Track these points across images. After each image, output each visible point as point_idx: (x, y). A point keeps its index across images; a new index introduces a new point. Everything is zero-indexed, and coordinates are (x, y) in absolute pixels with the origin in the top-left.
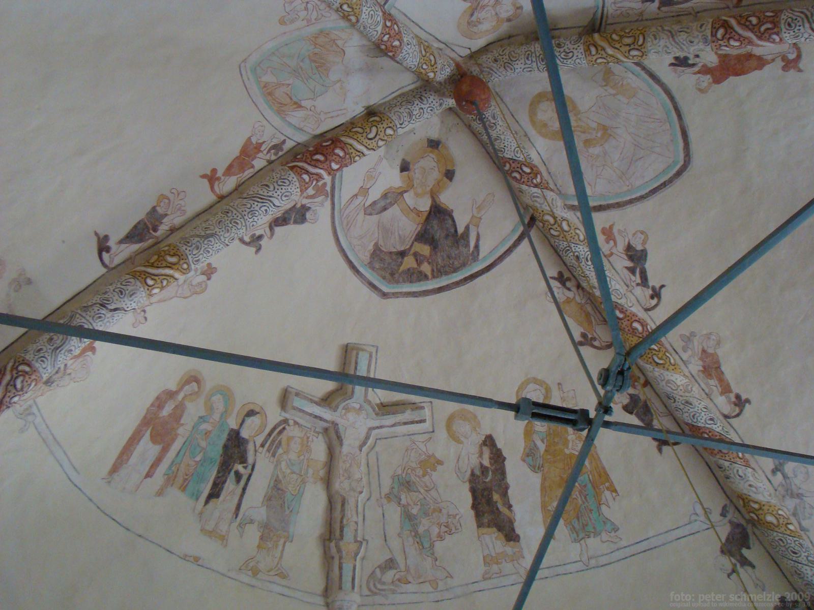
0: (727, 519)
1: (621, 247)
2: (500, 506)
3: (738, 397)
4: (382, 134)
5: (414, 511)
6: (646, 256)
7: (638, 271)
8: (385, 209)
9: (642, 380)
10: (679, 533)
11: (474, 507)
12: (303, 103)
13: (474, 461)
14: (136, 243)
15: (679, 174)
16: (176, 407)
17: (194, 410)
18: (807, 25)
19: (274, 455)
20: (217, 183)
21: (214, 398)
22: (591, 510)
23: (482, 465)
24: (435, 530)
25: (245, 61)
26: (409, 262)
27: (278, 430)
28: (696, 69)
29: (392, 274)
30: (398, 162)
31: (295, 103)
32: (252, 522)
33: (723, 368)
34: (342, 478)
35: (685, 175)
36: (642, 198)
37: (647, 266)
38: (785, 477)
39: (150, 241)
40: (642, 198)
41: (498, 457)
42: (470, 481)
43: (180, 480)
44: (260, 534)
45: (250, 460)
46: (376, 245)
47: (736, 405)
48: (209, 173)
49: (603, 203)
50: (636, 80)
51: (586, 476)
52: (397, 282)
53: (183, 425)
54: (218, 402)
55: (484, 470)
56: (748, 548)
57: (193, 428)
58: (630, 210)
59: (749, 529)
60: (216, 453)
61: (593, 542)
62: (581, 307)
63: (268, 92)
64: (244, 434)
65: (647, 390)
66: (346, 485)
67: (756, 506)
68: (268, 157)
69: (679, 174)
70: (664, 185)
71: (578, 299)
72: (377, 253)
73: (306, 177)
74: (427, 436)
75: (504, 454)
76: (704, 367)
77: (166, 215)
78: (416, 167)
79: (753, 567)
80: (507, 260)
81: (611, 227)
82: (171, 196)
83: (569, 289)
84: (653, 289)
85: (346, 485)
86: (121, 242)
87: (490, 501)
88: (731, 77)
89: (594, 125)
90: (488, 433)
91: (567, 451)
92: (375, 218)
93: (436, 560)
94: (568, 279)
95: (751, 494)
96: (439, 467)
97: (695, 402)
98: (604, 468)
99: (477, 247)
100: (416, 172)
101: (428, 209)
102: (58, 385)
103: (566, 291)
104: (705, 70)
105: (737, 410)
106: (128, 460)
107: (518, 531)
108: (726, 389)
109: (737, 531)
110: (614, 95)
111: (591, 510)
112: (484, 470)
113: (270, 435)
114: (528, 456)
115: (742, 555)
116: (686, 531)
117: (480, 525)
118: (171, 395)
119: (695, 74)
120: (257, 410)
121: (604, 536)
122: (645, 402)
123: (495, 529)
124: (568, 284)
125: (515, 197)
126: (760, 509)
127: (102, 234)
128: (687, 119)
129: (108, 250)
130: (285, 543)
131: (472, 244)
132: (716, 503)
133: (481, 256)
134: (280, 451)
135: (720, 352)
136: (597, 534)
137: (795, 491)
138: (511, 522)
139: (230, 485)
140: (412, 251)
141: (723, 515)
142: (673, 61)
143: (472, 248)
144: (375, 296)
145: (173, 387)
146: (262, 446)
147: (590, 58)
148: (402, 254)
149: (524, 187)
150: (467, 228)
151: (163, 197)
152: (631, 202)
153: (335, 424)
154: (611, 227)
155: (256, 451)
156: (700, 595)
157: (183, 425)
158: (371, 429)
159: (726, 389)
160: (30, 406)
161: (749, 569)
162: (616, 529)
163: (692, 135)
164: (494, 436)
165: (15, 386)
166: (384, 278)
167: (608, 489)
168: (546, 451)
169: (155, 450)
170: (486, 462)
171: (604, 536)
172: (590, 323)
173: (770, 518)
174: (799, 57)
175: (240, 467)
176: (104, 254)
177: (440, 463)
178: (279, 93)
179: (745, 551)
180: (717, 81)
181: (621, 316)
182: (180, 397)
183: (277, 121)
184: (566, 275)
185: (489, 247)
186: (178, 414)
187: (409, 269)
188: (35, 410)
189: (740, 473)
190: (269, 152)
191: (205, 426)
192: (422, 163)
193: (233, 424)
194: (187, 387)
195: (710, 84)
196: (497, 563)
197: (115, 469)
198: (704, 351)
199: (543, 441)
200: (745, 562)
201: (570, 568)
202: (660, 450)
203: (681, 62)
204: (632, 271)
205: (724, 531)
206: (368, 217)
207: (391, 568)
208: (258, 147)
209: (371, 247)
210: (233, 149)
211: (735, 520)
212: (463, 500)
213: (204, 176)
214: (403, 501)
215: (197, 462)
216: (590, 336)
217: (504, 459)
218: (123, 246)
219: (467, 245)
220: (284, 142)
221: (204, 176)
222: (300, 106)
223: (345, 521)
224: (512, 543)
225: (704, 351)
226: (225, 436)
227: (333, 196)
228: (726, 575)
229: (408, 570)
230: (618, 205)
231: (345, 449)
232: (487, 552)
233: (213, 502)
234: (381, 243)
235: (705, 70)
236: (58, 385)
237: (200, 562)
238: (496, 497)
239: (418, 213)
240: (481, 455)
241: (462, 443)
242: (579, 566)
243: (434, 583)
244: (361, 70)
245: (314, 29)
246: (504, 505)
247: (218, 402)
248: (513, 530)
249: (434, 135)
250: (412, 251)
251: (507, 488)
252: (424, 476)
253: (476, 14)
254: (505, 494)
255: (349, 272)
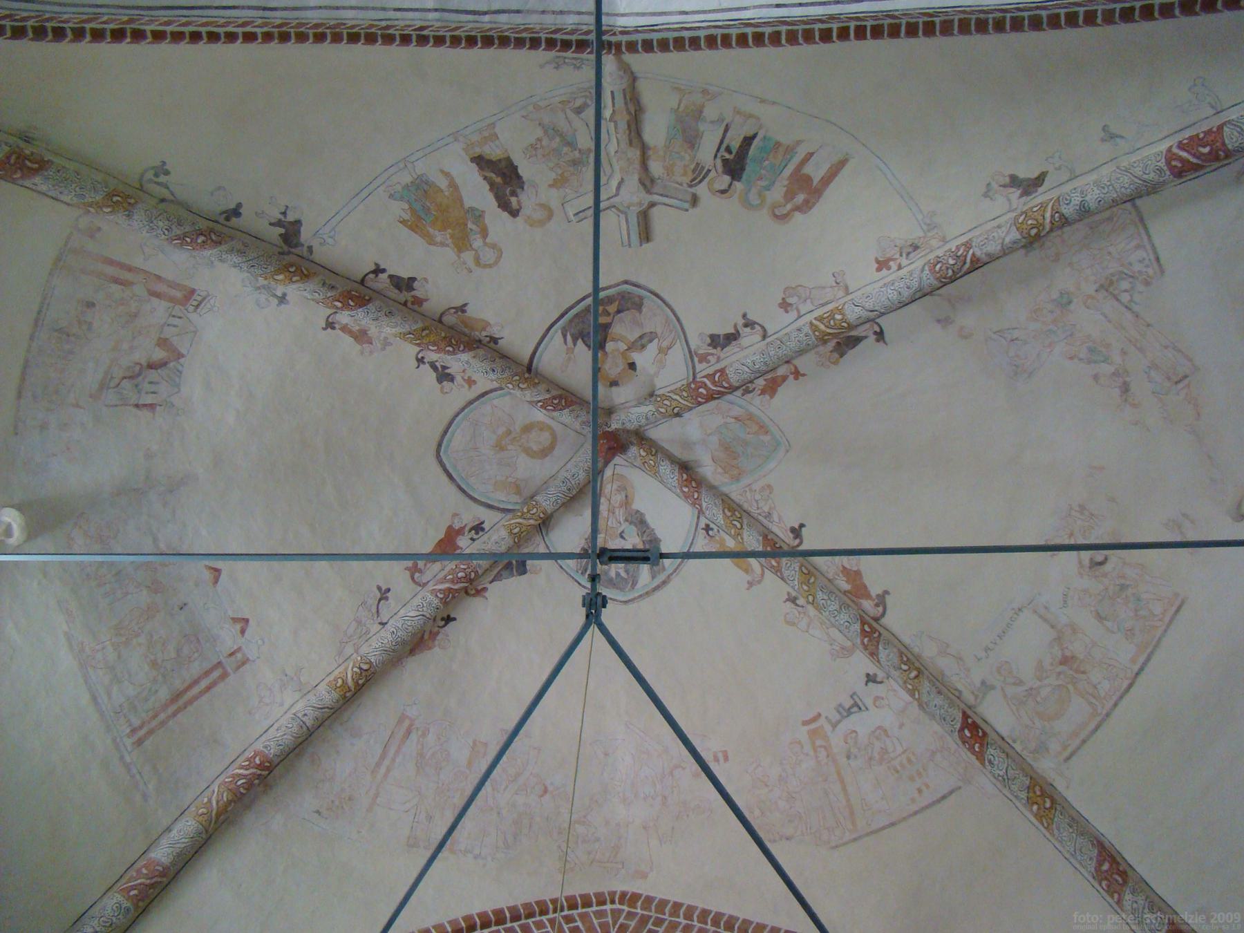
0: (306, 245)
1: (458, 379)
2: (493, 175)
3: (333, 328)
4: (669, 409)
5: (565, 149)
6: (438, 380)
7: (440, 369)
8: (641, 337)
9: (409, 304)
10: (338, 218)
11: (516, 168)
12: (733, 420)
13: (523, 197)
14: (851, 336)
15: (440, 445)
16: (792, 199)
17: (777, 194)
18: (428, 616)
19: (698, 164)
20: (793, 370)
21: (758, 202)
22: (416, 200)
23: (517, 196)
24: (545, 143)
25: (787, 451)
26: (612, 308)
27: (697, 181)
28: (467, 529)
29: (623, 297)
30: (638, 367)
31: (740, 421)
32: (712, 122)
33: (352, 339)
34: (635, 157)
35: (434, 447)
36: (457, 415)
37: (434, 375)
38: (275, 296)
39: (842, 336)
40: (457, 415)
41: (504, 205)
42: (523, 182)
43: (781, 150)
44: (704, 114)
45: (719, 162)
46: (640, 312)
47: (333, 323)
48: (800, 377)
49: (483, 399)
50: (501, 497)
51: (428, 221)
52: (619, 294)
53: (785, 186)
54: (754, 198)
55: (514, 194)
56: (281, 235)
57: (774, 183)
58: (462, 403)
59: (286, 248)
60: (750, 167)
61: (407, 179)
62: (472, 329)
63: (763, 429)
64: (727, 179)
65: (403, 300)
66: (630, 154)
67: (295, 279)
68: (754, 386)
69: (440, 445)
70: (445, 432)
71: (477, 333)
72: (639, 306)
73: (726, 385)
74: (568, 198)
75: (500, 210)
76: (366, 334)
77: (831, 352)
78: (622, 367)
79: (271, 224)
80: (539, 337)
81: (470, 387)
82: (828, 363)
83: (486, 336)
84: (424, 363)
85: (630, 154)
86: (866, 337)
87: (503, 175)
88: (443, 536)
89: (509, 448)
90: (518, 219)
91: (449, 231)
92: (647, 330)
93: (540, 124)
94: (489, 342)
95: (302, 285)
96: (551, 182)
97: (371, 322)
98: (416, 233)
99: (565, 336)
100: (622, 365)
101: (607, 345)
102: (906, 241)
103: (488, 334)
104: (460, 532)
105: (330, 320)
106: (830, 168)
107: (474, 165)
108: (345, 329)
109: (295, 242)
110: (507, 478)
111: (416, 200)
112: (514, 194)
113: (704, 178)
114: (480, 216)
115: (283, 226)
116: (334, 222)
117: (508, 160)
118: (797, 208)
119: (466, 525)
120: (718, 194)
121: (399, 188)
122: (401, 292)
123: (494, 160)
124: (488, 339)
125: (552, 383)
126: (291, 279)
127: (881, 343)
128: (454, 489)
129: (875, 333)
130: (678, 108)
131: (569, 338)
132: (320, 254)
133: (560, 331)
134: (692, 167)
135: (358, 347)
136: (407, 187)
137: (263, 290)
138: (481, 168)
139: (735, 145)
140: (612, 316)
141: (310, 249)
142: (483, 526)
143: (568, 334)
144: (633, 279)
145: (797, 215)
146: (709, 171)
147: (542, 509)
148: (619, 312)
149: (548, 396)
150: (575, 345)
151: (836, 363)
152: (463, 409)
153: (649, 192)
154: (470, 387)
155: (715, 166)
156: (1109, 917)
157: (785, 186)
158: (616, 195)
159: (345, 329)
160: (929, 231)
161: (273, 221)
162: (391, 196)
163: (444, 478)
164: (512, 218)
165: (953, 271)
166: (629, 293)
167: (409, 221)
168: (466, 225)
169: (808, 170)
170: (513, 200)
171: (399, 188)
172: (463, 322)
173: (281, 277)
174: (413, 578)
175: (727, 156)
176: (878, 330)
177: (550, 186)
178: (755, 428)
179: (282, 231)
180: (450, 528)
181: (447, 349)
182: (789, 207)
183: (753, 409)
184: (492, 345)
185: (556, 338)
186: (789, 195)
187: (611, 303)
188: (925, 227)
189: (317, 294)
190: (754, 389)
191: (763, 183)
192: (619, 370)
193: (738, 186)
194: (785, 212)
195: (453, 523)
196: (485, 137)
197: (842, 163)
198: (371, 343)
199: (471, 230)
200: (279, 224)
201: (420, 154)
202: (376, 264)
203: (478, 528)
204: (444, 368)
205: (305, 235)
206: (652, 330)
207: (579, 108)
208: (763, 392)
209: (644, 310)
210: (781, 390)
211: (300, 248)
212: (525, 169)
213: (804, 375)
214: (576, 153)
215: (767, 159)
216: (460, 313)
217: (499, 206)
218: (863, 334)
219: (572, 335)
220: (743, 395)
221: (804, 375)
222: (736, 418)
223: (627, 132)
224: (476, 155)
225: (371, 343)
226: (745, 176)
227: (690, 352)
228: (290, 206)
229: (563, 110)
230: (471, 403)
231: (636, 177)
232: (497, 142)
233: (751, 133)
234: (637, 314)
235: (460, 532)
236: (906, 241)
237: (759, 100)
238: (499, 180)
239: (613, 340)
240: (519, 202)
241: (536, 205)
242: (413, 158)
243: (537, 108)
244: (694, 444)
245: (745, 481)
246: (491, 178)
247: (754, 198)
248: (477, 164)
249: (614, 389)
250: (612, 316)
251: (491, 190)
252: (563, 173)
253: (624, 496)
254: (492, 186)
255: (658, 292)
